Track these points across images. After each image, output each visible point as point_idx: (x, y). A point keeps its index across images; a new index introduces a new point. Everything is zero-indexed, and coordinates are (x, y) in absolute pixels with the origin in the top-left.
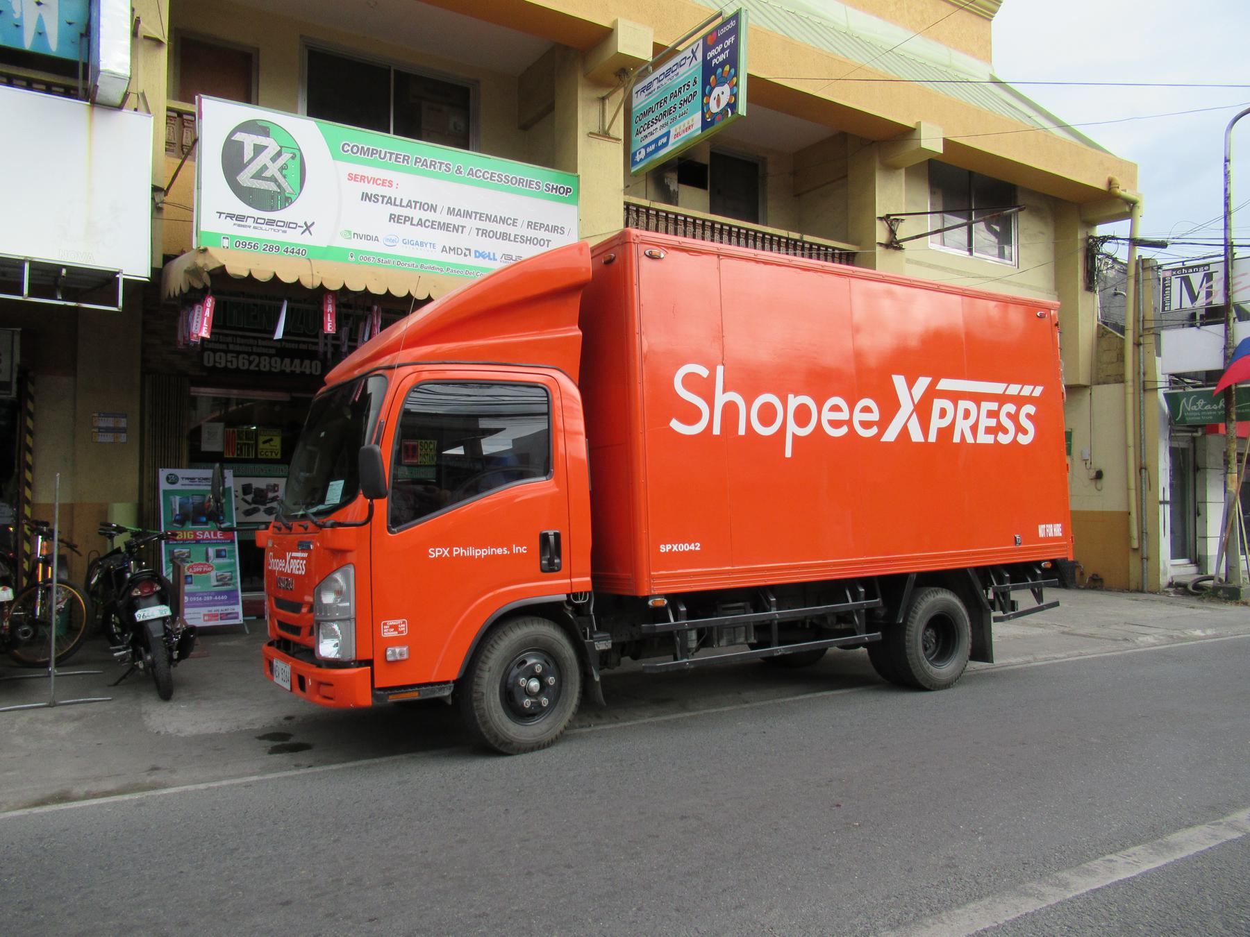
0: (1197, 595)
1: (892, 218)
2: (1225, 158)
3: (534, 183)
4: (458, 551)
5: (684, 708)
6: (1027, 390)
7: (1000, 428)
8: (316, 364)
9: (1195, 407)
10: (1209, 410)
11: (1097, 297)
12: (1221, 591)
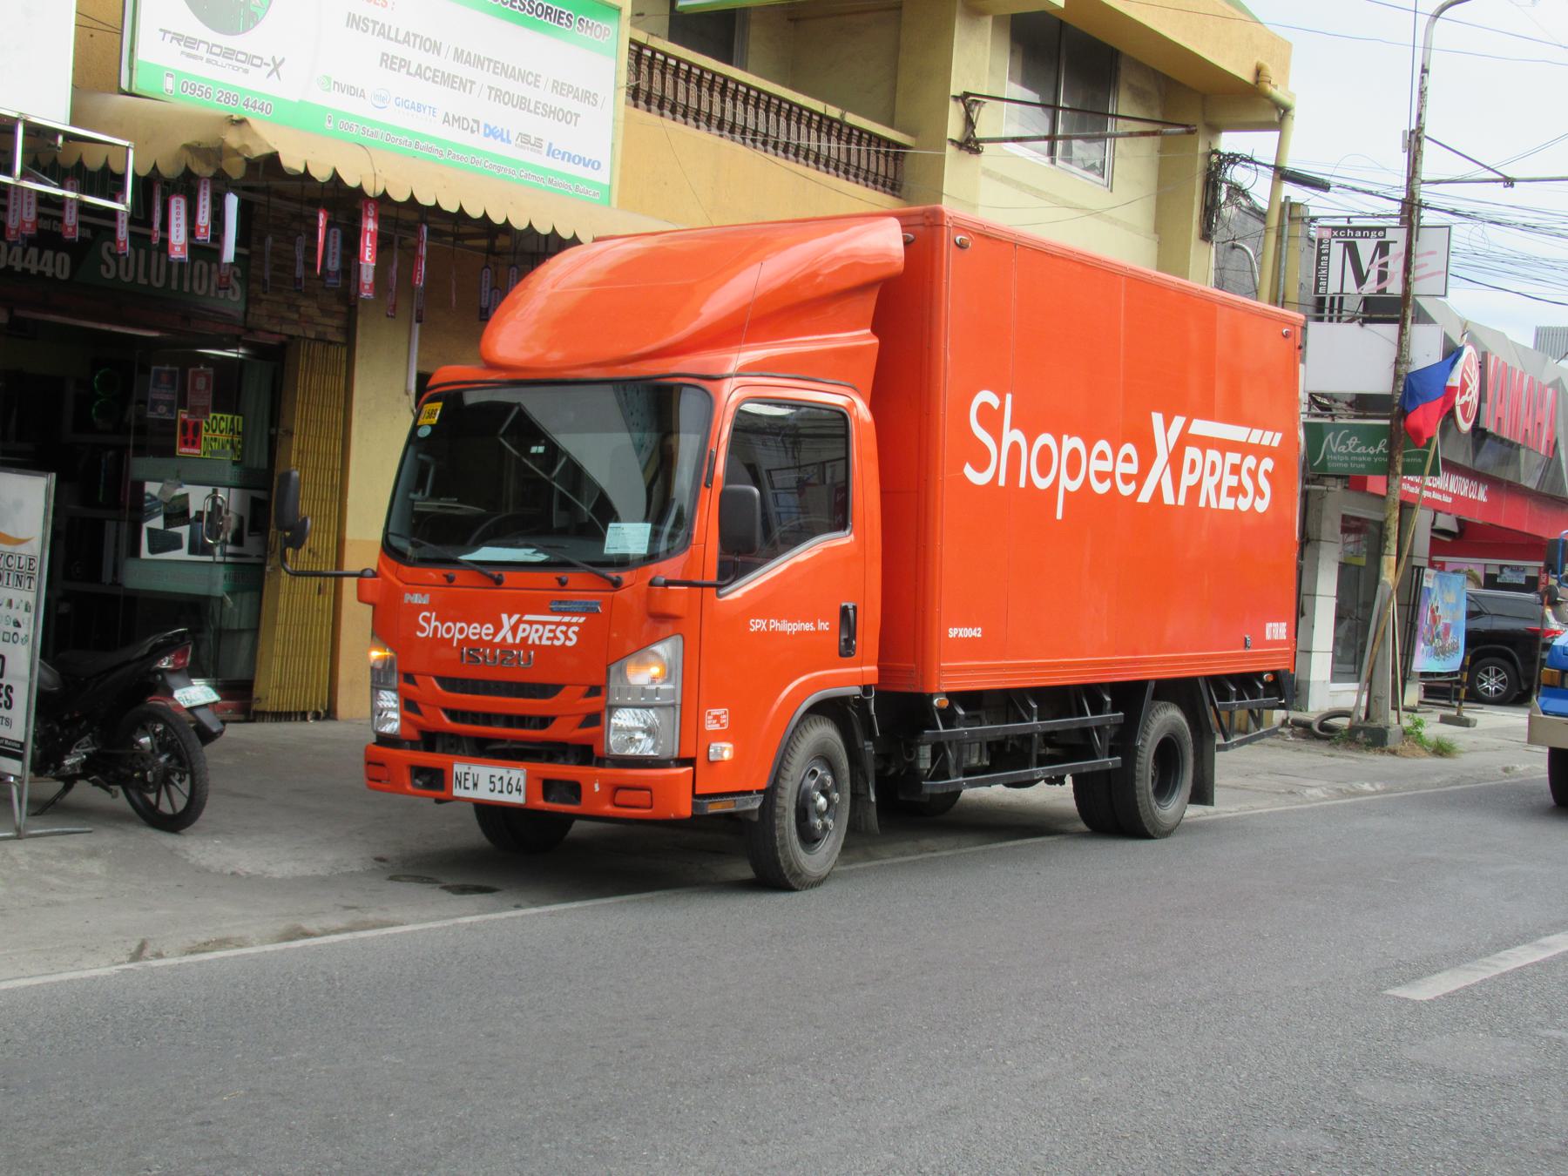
0: (1327, 738)
1: (971, 98)
2: (1423, 66)
3: (565, 16)
4: (775, 624)
5: (871, 858)
6: (1256, 436)
7: (556, 637)
8: (63, 259)
9: (1344, 447)
10: (1362, 455)
11: (1213, 250)
12: (1362, 733)
